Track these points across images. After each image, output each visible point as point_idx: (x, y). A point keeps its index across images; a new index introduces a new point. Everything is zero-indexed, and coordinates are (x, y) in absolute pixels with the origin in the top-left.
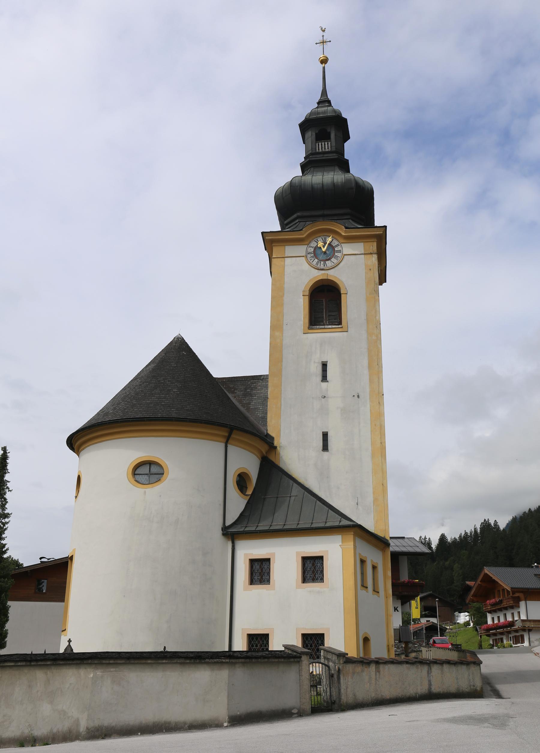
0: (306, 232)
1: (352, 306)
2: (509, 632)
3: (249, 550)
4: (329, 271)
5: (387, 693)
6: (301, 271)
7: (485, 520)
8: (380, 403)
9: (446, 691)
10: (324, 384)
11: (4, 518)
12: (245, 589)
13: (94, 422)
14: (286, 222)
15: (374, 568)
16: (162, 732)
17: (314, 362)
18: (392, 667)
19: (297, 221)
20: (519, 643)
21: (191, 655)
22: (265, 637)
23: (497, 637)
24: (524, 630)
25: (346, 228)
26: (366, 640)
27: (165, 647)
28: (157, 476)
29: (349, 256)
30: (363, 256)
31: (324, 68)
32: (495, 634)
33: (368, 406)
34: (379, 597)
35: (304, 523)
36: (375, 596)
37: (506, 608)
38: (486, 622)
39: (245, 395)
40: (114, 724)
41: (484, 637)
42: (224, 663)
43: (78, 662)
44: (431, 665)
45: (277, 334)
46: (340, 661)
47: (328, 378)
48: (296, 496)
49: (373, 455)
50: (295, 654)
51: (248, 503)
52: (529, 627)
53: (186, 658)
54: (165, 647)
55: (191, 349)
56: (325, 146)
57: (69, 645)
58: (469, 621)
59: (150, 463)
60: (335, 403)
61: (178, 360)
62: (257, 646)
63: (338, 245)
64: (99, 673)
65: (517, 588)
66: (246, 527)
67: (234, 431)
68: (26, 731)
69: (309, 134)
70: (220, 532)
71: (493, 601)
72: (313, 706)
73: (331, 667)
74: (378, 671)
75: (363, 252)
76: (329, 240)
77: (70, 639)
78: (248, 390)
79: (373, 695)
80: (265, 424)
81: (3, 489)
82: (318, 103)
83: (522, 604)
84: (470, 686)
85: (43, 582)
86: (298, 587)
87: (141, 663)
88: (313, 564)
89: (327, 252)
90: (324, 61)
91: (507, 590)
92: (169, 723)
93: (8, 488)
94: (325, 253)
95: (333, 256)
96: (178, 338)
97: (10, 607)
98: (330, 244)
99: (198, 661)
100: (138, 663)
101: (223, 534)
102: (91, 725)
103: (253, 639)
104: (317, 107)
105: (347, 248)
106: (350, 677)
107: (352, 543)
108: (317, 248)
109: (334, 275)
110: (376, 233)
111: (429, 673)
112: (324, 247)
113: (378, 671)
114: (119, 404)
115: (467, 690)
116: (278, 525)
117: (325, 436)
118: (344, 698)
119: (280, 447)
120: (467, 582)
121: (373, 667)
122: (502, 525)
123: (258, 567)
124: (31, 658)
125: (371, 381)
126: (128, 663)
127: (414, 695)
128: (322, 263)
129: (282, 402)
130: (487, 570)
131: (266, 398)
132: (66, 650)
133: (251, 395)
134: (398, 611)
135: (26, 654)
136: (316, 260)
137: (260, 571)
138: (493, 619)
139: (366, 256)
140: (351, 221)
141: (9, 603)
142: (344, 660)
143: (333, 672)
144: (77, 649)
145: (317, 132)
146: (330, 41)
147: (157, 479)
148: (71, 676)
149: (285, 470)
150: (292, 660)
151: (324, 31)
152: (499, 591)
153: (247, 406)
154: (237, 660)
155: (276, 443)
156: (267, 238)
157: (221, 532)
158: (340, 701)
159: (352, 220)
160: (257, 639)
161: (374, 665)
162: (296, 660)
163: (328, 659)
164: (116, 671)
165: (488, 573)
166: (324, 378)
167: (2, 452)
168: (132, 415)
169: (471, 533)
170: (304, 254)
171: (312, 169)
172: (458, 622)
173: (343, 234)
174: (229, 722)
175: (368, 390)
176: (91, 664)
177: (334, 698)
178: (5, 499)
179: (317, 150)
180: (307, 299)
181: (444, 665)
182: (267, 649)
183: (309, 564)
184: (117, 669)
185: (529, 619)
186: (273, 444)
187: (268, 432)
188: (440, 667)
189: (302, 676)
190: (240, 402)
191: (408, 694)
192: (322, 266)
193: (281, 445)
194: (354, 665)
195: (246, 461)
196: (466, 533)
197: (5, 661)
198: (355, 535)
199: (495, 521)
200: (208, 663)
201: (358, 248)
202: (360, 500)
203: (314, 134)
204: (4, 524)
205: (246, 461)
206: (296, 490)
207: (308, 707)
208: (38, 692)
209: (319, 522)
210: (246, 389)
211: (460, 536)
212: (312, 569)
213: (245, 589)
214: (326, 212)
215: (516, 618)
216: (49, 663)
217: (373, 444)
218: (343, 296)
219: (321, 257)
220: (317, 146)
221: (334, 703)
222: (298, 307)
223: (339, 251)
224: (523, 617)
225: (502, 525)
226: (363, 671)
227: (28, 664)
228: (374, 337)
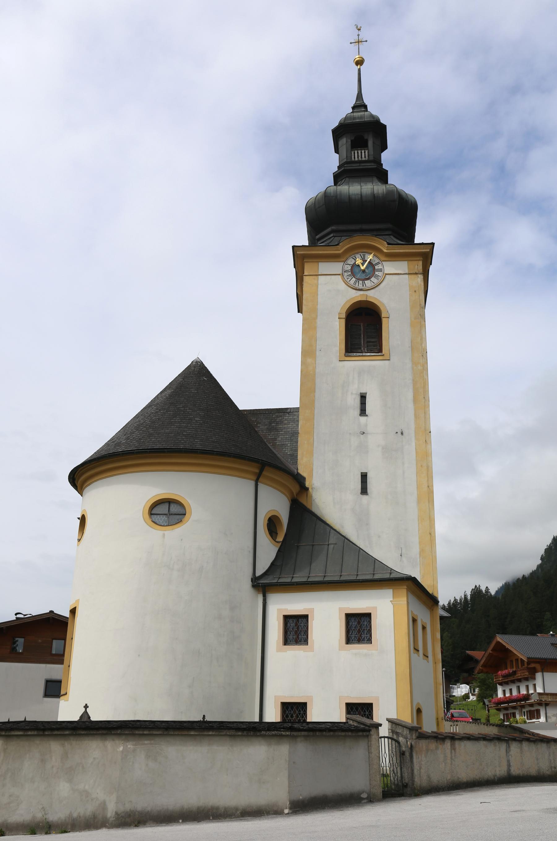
0: (343, 247)
1: (394, 331)
2: (523, 707)
3: (283, 605)
5: (464, 775)
6: (335, 290)
7: (476, 586)
8: (427, 442)
10: (363, 419)
12: (278, 650)
13: (104, 453)
14: (317, 237)
15: (424, 628)
16: (209, 819)
17: (352, 393)
19: (332, 235)
20: (534, 718)
22: (302, 707)
23: (509, 712)
24: (540, 704)
25: (389, 244)
26: (419, 711)
27: (204, 716)
28: (178, 517)
29: (391, 276)
30: (407, 276)
31: (359, 70)
32: (506, 709)
33: (413, 444)
34: (428, 662)
35: (348, 575)
36: (425, 661)
37: (520, 680)
38: (497, 695)
40: (149, 809)
41: (493, 711)
42: (284, 736)
43: (104, 732)
44: (510, 742)
45: (309, 360)
46: (412, 735)
47: (368, 412)
48: (336, 544)
49: (419, 501)
50: (362, 726)
51: (279, 551)
52: (545, 701)
53: (238, 729)
54: (204, 716)
55: (211, 375)
56: (361, 155)
57: (86, 712)
58: (469, 693)
59: (169, 502)
60: (375, 441)
61: (197, 387)
62: (292, 716)
63: (378, 263)
64: (130, 746)
65: (534, 658)
67: (266, 468)
68: (39, 816)
69: (343, 141)
70: (249, 583)
71: (505, 672)
73: (401, 743)
74: (453, 748)
75: (407, 272)
77: (86, 704)
78: (273, 425)
82: (353, 108)
83: (539, 675)
85: (17, 641)
86: (341, 649)
87: (182, 735)
88: (359, 623)
89: (367, 271)
90: (359, 63)
91: (521, 659)
92: (217, 808)
94: (364, 271)
96: (197, 362)
98: (370, 262)
99: (252, 733)
100: (178, 735)
101: (254, 586)
102: (121, 809)
103: (287, 708)
104: (352, 112)
105: (389, 267)
106: (423, 756)
107: (405, 599)
108: (355, 266)
109: (373, 296)
110: (422, 251)
111: (508, 751)
112: (363, 264)
113: (453, 748)
115: (548, 773)
116: (317, 576)
117: (364, 477)
118: (417, 779)
119: (312, 489)
120: (468, 652)
121: (448, 743)
122: (493, 592)
123: (293, 625)
124: (43, 726)
125: (416, 416)
126: (166, 735)
127: (492, 778)
128: (361, 282)
129: (315, 437)
130: (499, 638)
131: (295, 434)
132: (81, 717)
133: (277, 430)
135: (36, 722)
136: (354, 279)
137: (296, 630)
138: (504, 692)
139: (410, 276)
140: (392, 237)
142: (417, 734)
143: (404, 749)
144: (96, 716)
145: (353, 138)
146: (366, 41)
147: (178, 520)
148: (94, 749)
149: (318, 515)
150: (361, 734)
151: (359, 30)
152: (512, 661)
155: (307, 484)
156: (298, 252)
157: (251, 583)
158: (413, 784)
162: (365, 734)
163: (397, 734)
165: (501, 641)
166: (363, 412)
169: (461, 600)
170: (340, 272)
171: (347, 179)
172: (454, 694)
173: (385, 251)
174: (290, 809)
175: (413, 426)
176: (120, 734)
177: (406, 780)
179: (353, 159)
180: (343, 321)
181: (524, 742)
182: (305, 721)
184: (152, 742)
185: (547, 692)
186: (305, 484)
187: (299, 471)
188: (519, 745)
189: (371, 753)
191: (486, 777)
192: (360, 286)
193: (313, 486)
194: (427, 741)
195: (275, 503)
196: (455, 600)
197: (12, 729)
198: (409, 590)
199: (487, 587)
200: (264, 736)
201: (402, 266)
202: (404, 551)
203: (350, 141)
206: (333, 539)
207: (379, 791)
208: (53, 767)
209: (366, 574)
210: (270, 423)
211: (449, 603)
212: (358, 628)
213: (278, 650)
214: (365, 227)
215: (531, 691)
216: (67, 732)
217: (419, 487)
218: (384, 321)
220: (353, 154)
221: (405, 786)
222: (334, 331)
223: (380, 270)
224: (540, 690)
225: (493, 592)
226: (437, 748)
227: (41, 733)
228: (420, 367)
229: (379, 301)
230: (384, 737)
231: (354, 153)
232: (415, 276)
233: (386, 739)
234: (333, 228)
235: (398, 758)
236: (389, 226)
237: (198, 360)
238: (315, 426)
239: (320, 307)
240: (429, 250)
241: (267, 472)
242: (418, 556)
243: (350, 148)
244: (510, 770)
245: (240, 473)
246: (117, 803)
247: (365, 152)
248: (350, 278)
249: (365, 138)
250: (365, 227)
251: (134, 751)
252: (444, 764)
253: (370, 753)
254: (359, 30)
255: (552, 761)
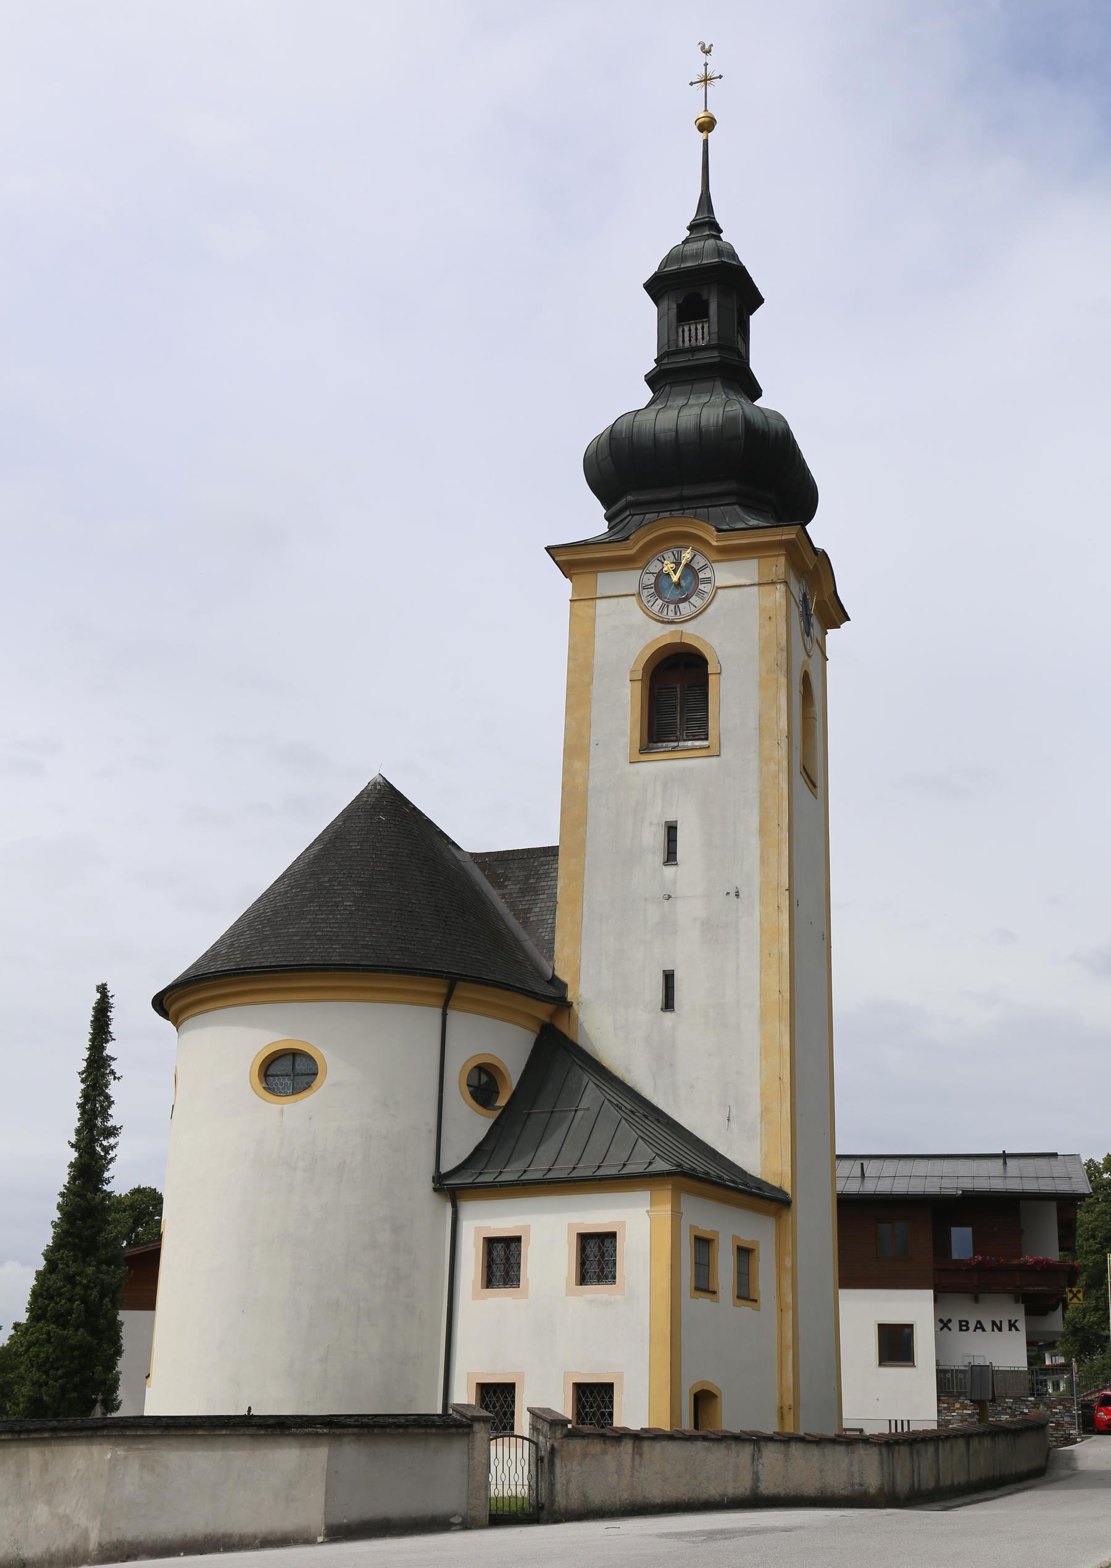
3: (483, 1220)
4: (686, 625)
9: (792, 1493)
10: (669, 871)
11: (106, 1138)
12: (475, 1296)
17: (651, 824)
18: (671, 1447)
19: (627, 513)
21: (271, 1422)
29: (727, 590)
30: (756, 588)
31: (706, 143)
33: (757, 913)
39: (523, 892)
40: (142, 1538)
42: (321, 1434)
43: (89, 1433)
44: (762, 1443)
45: (577, 765)
46: (555, 1433)
48: (588, 1109)
56: (699, 334)
60: (690, 910)
63: (704, 567)
64: (120, 1452)
66: (480, 1174)
70: (430, 1185)
72: (494, 1512)
73: (540, 1444)
74: (638, 1452)
75: (756, 580)
76: (687, 555)
78: (532, 881)
79: (625, 1496)
80: (551, 957)
81: (104, 1075)
82: (691, 228)
84: (852, 1485)
86: (569, 1293)
89: (683, 584)
90: (707, 125)
92: (230, 1536)
93: (113, 1072)
94: (678, 585)
95: (695, 591)
97: (122, 1324)
98: (688, 566)
99: (278, 1431)
101: (435, 1190)
102: (107, 1538)
103: (488, 1393)
105: (724, 574)
106: (575, 1463)
107: (669, 1207)
108: (661, 576)
112: (675, 571)
113: (638, 1452)
114: (242, 934)
115: (844, 1493)
117: (669, 978)
121: (628, 1446)
127: (717, 1498)
128: (672, 607)
134: (1017, 1330)
136: (660, 602)
137: (503, 1261)
140: (737, 507)
141: (123, 1315)
146: (721, 77)
150: (454, 1430)
151: (707, 52)
153: (523, 916)
154: (345, 1431)
155: (570, 997)
157: (432, 1185)
159: (740, 505)
160: (592, 1393)
161: (631, 1442)
162: (461, 1430)
164: (147, 1449)
166: (671, 856)
167: (98, 996)
168: (257, 961)
173: (714, 543)
174: (326, 1536)
175: (757, 880)
177: (543, 1499)
178: (108, 1097)
183: (592, 1247)
184: (150, 1446)
188: (783, 1448)
190: (512, 906)
191: (704, 1496)
192: (671, 615)
193: (581, 999)
194: (585, 1441)
200: (295, 1435)
201: (745, 571)
204: (107, 1150)
205: (500, 1040)
206: (592, 1095)
207: (484, 1515)
210: (527, 878)
212: (596, 1257)
213: (475, 1296)
214: (688, 491)
216: (46, 1435)
219: (669, 594)
220: (681, 333)
222: (622, 704)
223: (708, 581)
226: (604, 1452)
227: (16, 1437)
229: (705, 642)
230: (523, 1438)
231: (683, 331)
232: (772, 587)
233: (526, 1443)
234: (630, 498)
235: (533, 1468)
236: (732, 485)
237: (380, 780)
238: (585, 888)
239: (598, 660)
240: (794, 536)
241: (462, 991)
242: (758, 1120)
243: (674, 319)
244: (758, 1487)
245: (415, 998)
246: (100, 1531)
247: (703, 328)
248: (653, 599)
249: (704, 298)
250: (688, 491)
251: (125, 1458)
252: (616, 1476)
253: (471, 1458)
254: (707, 52)
255: (857, 1474)
